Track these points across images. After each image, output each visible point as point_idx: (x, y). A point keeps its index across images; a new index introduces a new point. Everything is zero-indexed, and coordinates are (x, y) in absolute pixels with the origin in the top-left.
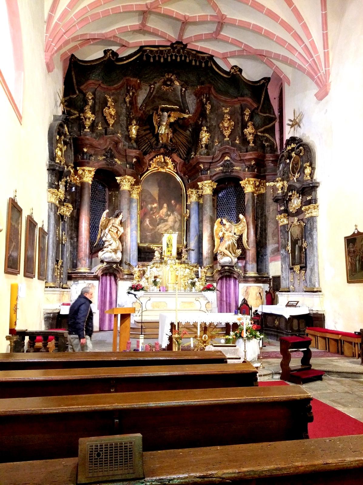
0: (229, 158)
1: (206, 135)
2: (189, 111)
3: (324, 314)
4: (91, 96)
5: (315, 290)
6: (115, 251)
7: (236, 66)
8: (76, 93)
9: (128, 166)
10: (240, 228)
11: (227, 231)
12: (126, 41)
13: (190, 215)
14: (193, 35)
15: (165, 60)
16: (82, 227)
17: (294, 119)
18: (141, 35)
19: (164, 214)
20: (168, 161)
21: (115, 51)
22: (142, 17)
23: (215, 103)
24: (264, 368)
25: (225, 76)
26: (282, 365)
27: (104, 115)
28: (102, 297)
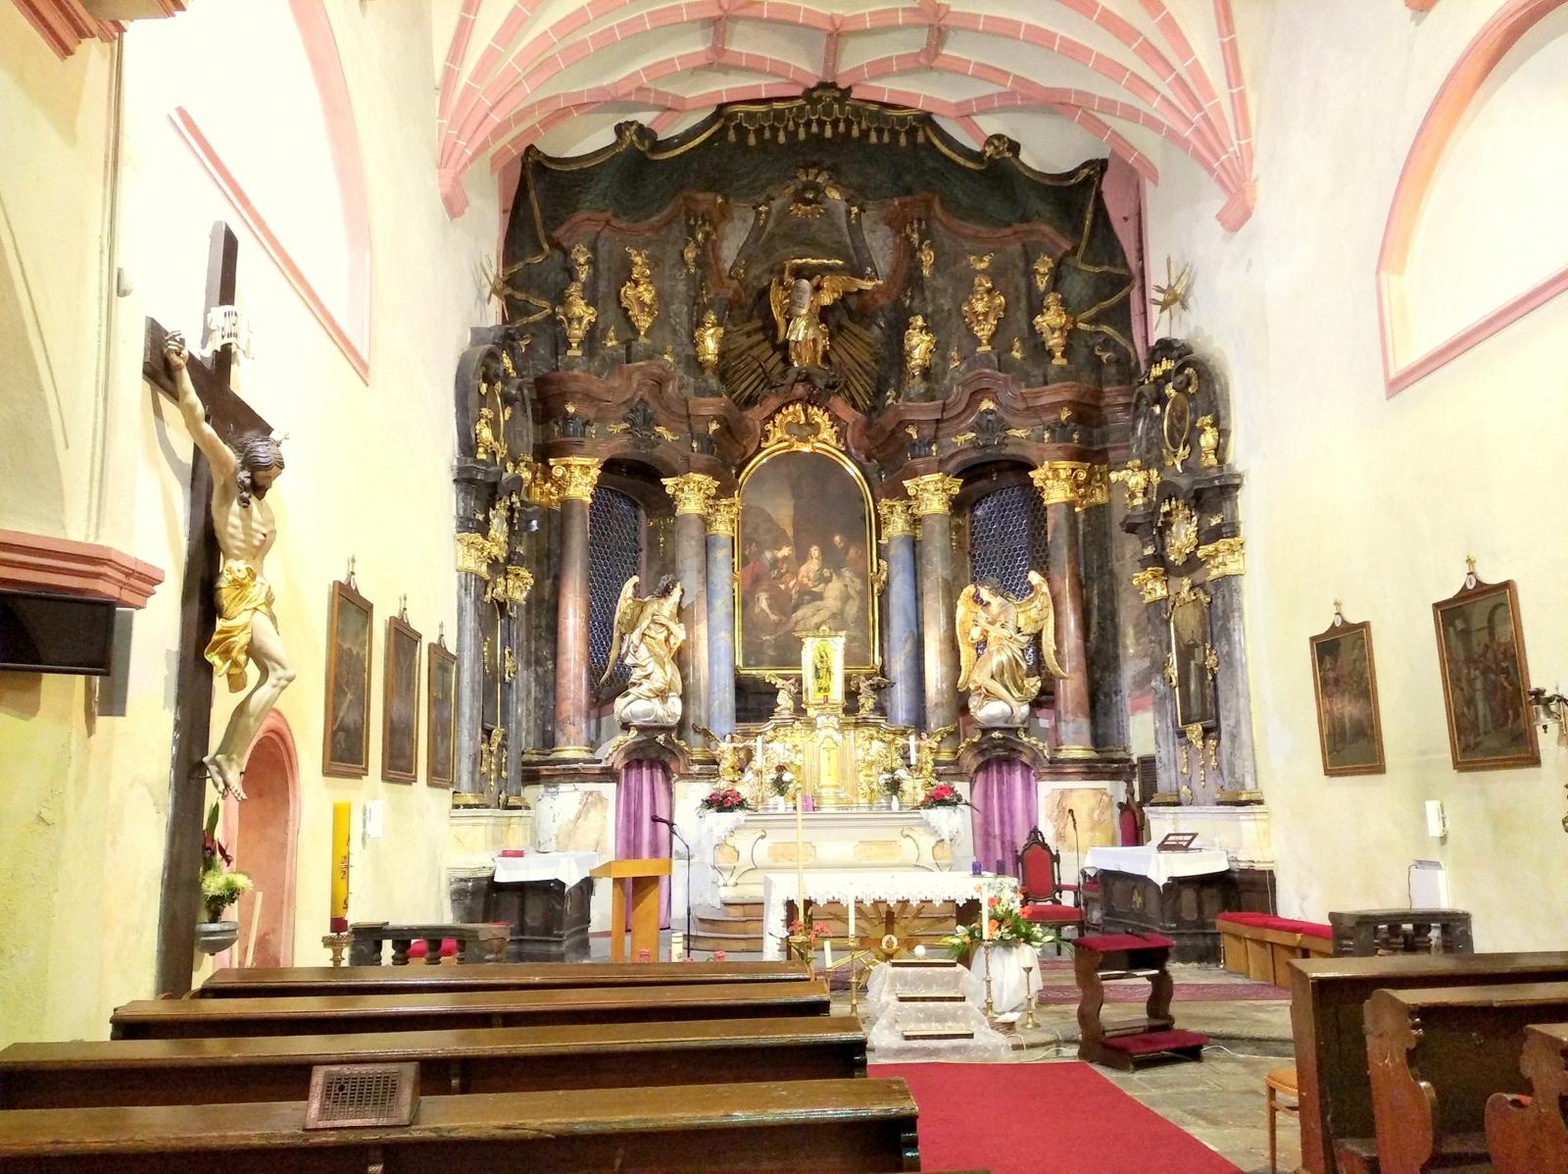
0: (992, 406)
1: (923, 341)
2: (875, 271)
3: (1271, 872)
4: (584, 254)
5: (1244, 798)
6: (662, 695)
7: (999, 137)
8: (540, 249)
9: (695, 445)
10: (1033, 613)
11: (992, 623)
12: (675, 96)
13: (888, 577)
14: (865, 62)
15: (792, 135)
16: (566, 628)
17: (1169, 286)
18: (721, 77)
19: (812, 575)
20: (817, 419)
21: (645, 125)
22: (713, 28)
23: (947, 243)
24: (1037, 1026)
25: (970, 165)
26: (1083, 1017)
27: (624, 305)
28: (628, 831)
